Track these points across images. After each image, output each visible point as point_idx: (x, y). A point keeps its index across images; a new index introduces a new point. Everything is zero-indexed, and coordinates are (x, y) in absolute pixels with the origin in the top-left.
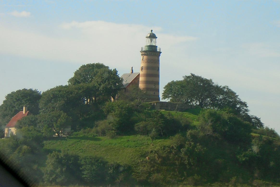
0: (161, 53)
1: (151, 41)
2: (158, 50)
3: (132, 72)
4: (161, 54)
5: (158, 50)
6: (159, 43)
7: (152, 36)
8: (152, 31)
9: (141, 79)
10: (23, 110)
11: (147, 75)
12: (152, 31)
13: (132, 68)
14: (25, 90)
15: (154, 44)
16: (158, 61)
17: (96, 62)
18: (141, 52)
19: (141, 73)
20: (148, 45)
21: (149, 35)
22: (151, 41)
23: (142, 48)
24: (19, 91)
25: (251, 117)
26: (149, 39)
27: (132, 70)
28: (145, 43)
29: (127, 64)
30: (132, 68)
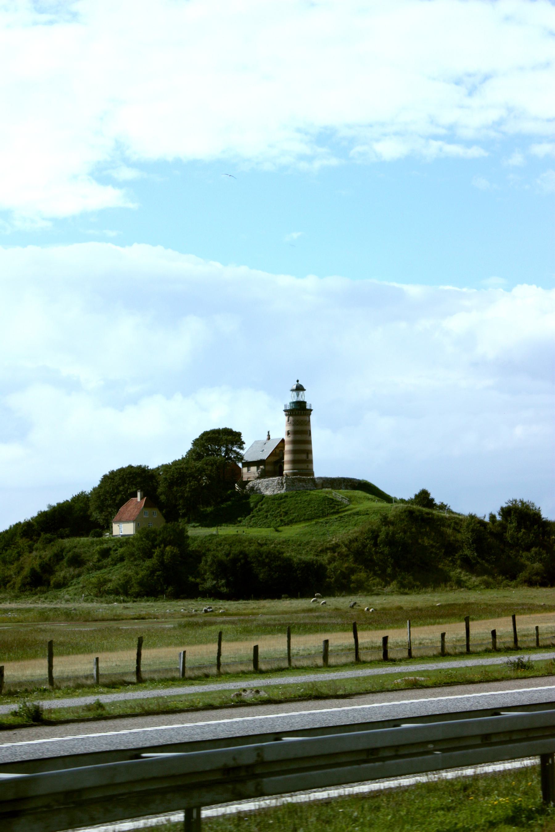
0: (311, 410)
1: (298, 395)
2: (308, 407)
3: (269, 439)
4: (312, 412)
5: (308, 407)
6: (307, 397)
7: (299, 388)
8: (298, 381)
9: (287, 447)
10: (137, 497)
11: (294, 442)
12: (298, 381)
13: (269, 432)
14: (130, 467)
15: (301, 399)
16: (307, 423)
17: (222, 427)
18: (285, 411)
19: (286, 439)
20: (295, 401)
21: (295, 387)
22: (298, 395)
23: (285, 406)
24: (121, 470)
25: (197, 524)
26: (295, 393)
27: (269, 435)
28: (291, 398)
29: (261, 428)
30: (269, 432)
